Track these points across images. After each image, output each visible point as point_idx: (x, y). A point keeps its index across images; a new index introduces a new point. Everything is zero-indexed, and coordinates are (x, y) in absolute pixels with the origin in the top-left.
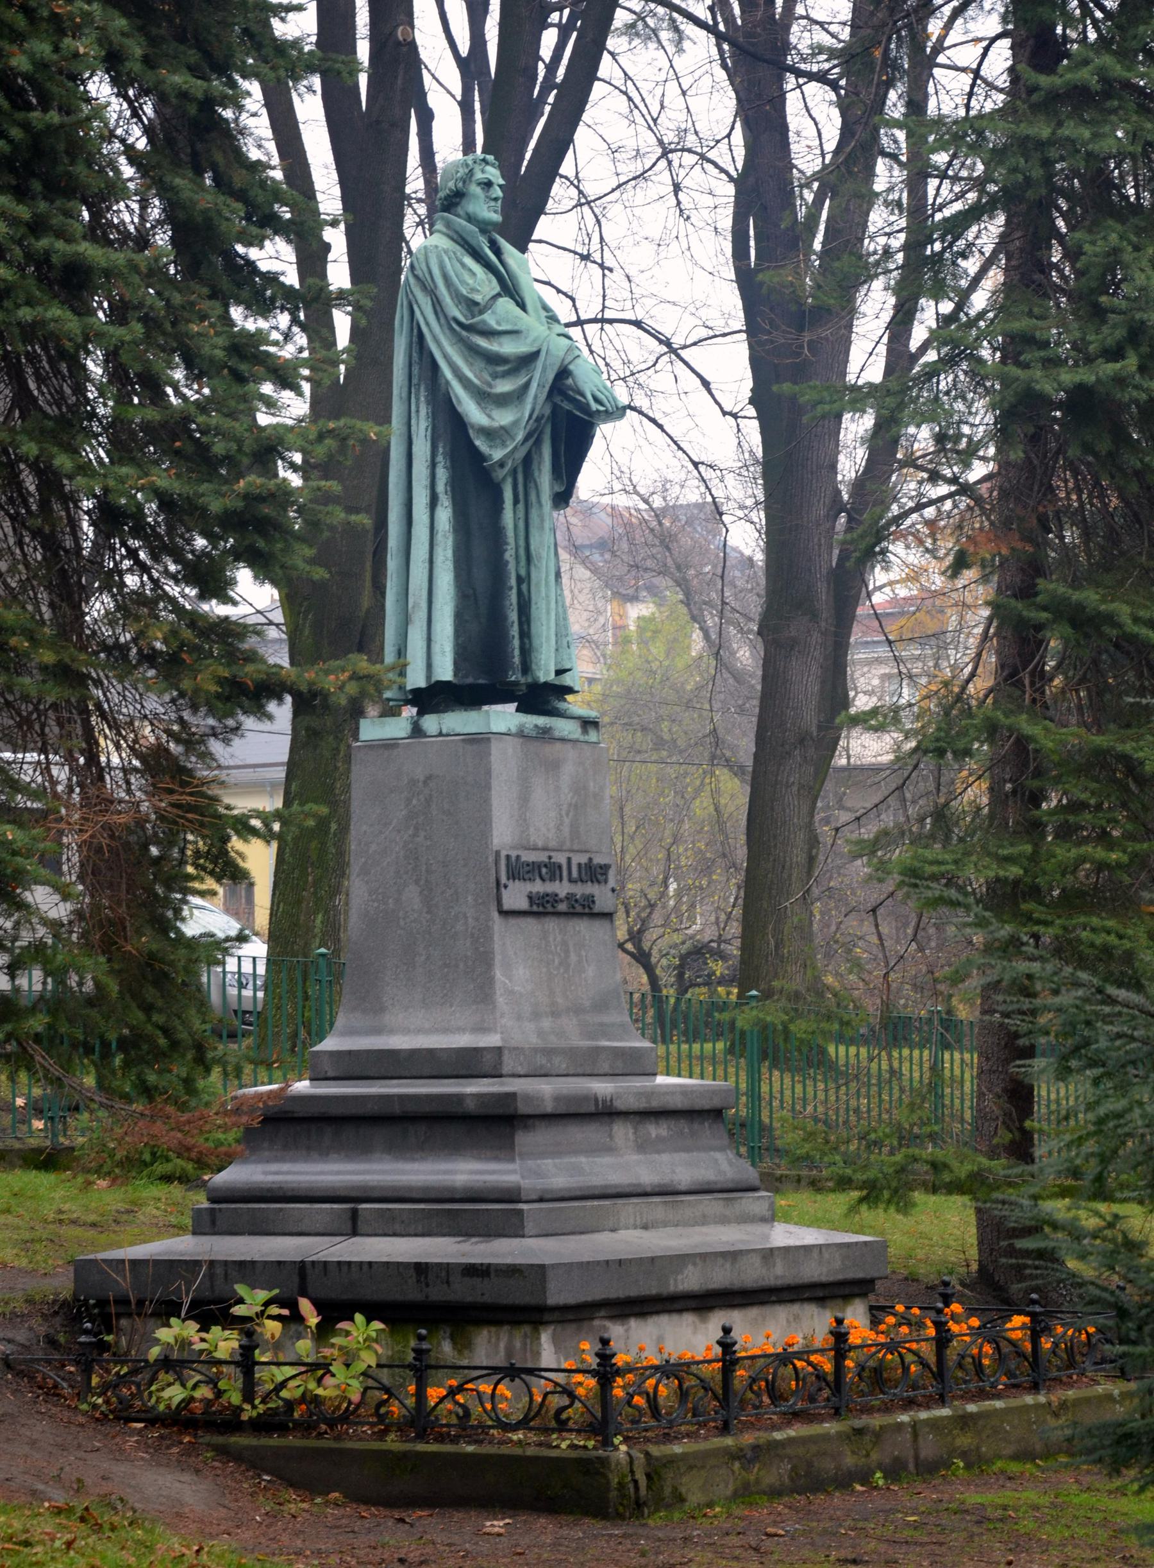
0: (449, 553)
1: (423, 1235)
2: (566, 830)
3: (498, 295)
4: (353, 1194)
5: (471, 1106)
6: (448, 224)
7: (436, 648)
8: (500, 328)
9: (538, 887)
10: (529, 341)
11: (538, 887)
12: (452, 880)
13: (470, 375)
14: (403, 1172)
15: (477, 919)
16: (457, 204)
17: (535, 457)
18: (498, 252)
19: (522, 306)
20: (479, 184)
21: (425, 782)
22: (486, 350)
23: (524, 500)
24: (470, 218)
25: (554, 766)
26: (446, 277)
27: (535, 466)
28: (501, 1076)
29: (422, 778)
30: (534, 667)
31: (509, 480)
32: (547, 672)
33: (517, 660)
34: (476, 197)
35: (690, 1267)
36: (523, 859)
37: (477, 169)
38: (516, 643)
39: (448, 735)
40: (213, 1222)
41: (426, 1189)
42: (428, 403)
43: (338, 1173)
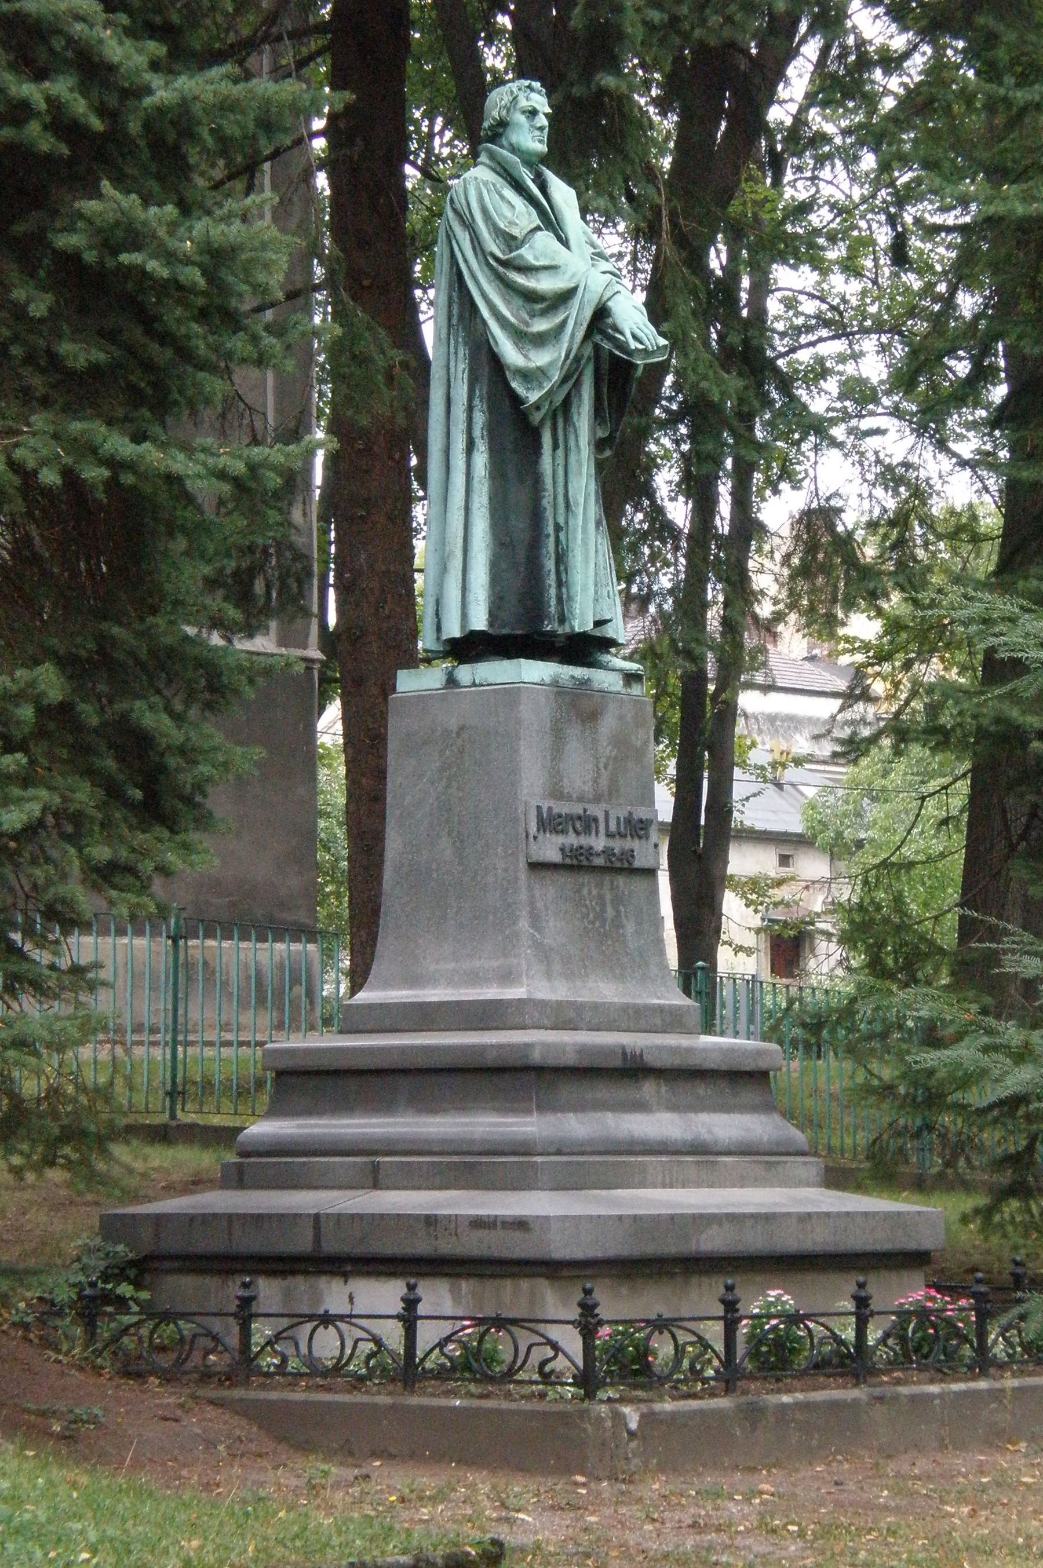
2: (604, 782)
3: (538, 228)
6: (492, 156)
7: (471, 598)
8: (537, 264)
9: (571, 840)
10: (567, 276)
11: (571, 840)
13: (507, 313)
15: (506, 870)
16: (500, 135)
18: (543, 187)
19: (565, 242)
20: (524, 112)
21: (458, 734)
24: (514, 149)
26: (485, 211)
27: (574, 410)
29: (455, 729)
31: (548, 424)
33: (552, 610)
35: (715, 1227)
38: (553, 592)
41: (444, 1141)
42: (466, 344)
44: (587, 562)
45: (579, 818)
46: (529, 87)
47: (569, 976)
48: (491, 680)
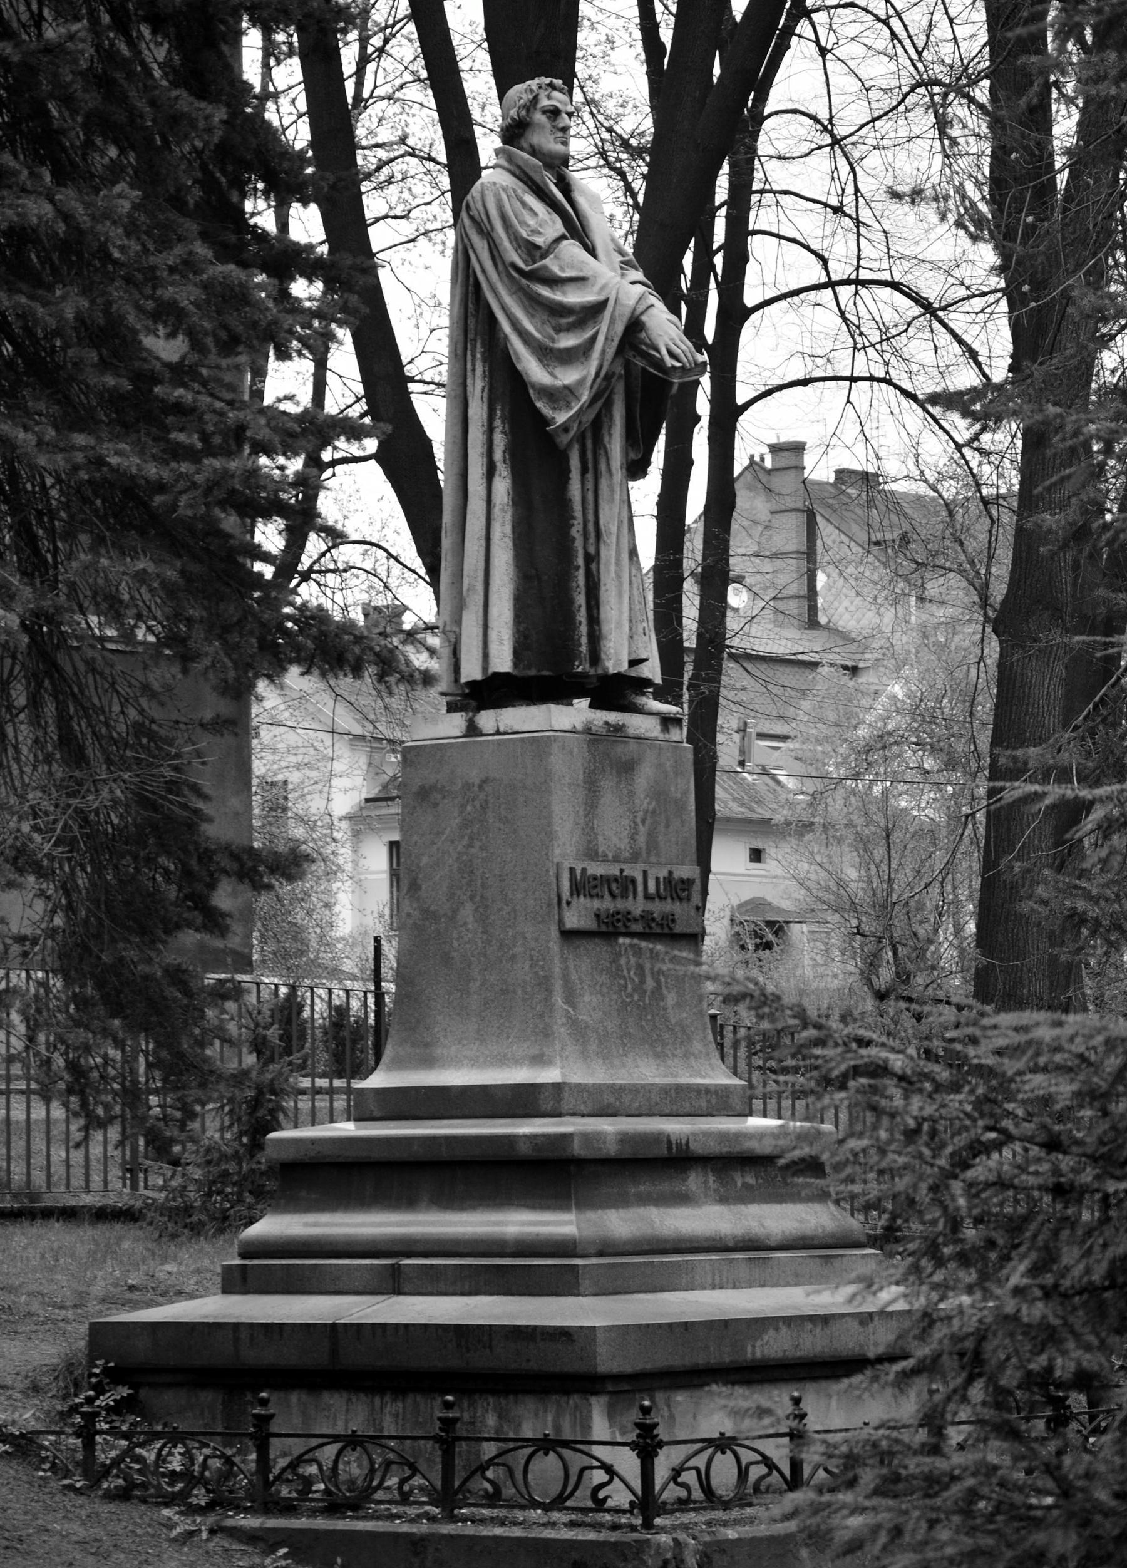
0: (508, 529)
1: (470, 1294)
2: (642, 839)
3: (563, 238)
4: (396, 1248)
5: (524, 1150)
7: (493, 635)
10: (596, 288)
11: (607, 904)
12: (510, 896)
14: (455, 1224)
17: (605, 419)
19: (592, 251)
20: (544, 112)
21: (480, 787)
22: (547, 298)
23: (592, 469)
24: (534, 152)
25: (627, 768)
26: (504, 218)
27: (605, 432)
28: (560, 1115)
29: (477, 782)
30: (603, 656)
32: (618, 662)
33: (584, 649)
34: (541, 127)
35: (771, 1332)
36: (590, 872)
37: (543, 94)
38: (584, 629)
39: (506, 733)
40: (244, 1279)
43: (380, 1225)
44: (620, 595)
45: (616, 880)
46: (551, 86)
47: (606, 1057)
48: (516, 728)
